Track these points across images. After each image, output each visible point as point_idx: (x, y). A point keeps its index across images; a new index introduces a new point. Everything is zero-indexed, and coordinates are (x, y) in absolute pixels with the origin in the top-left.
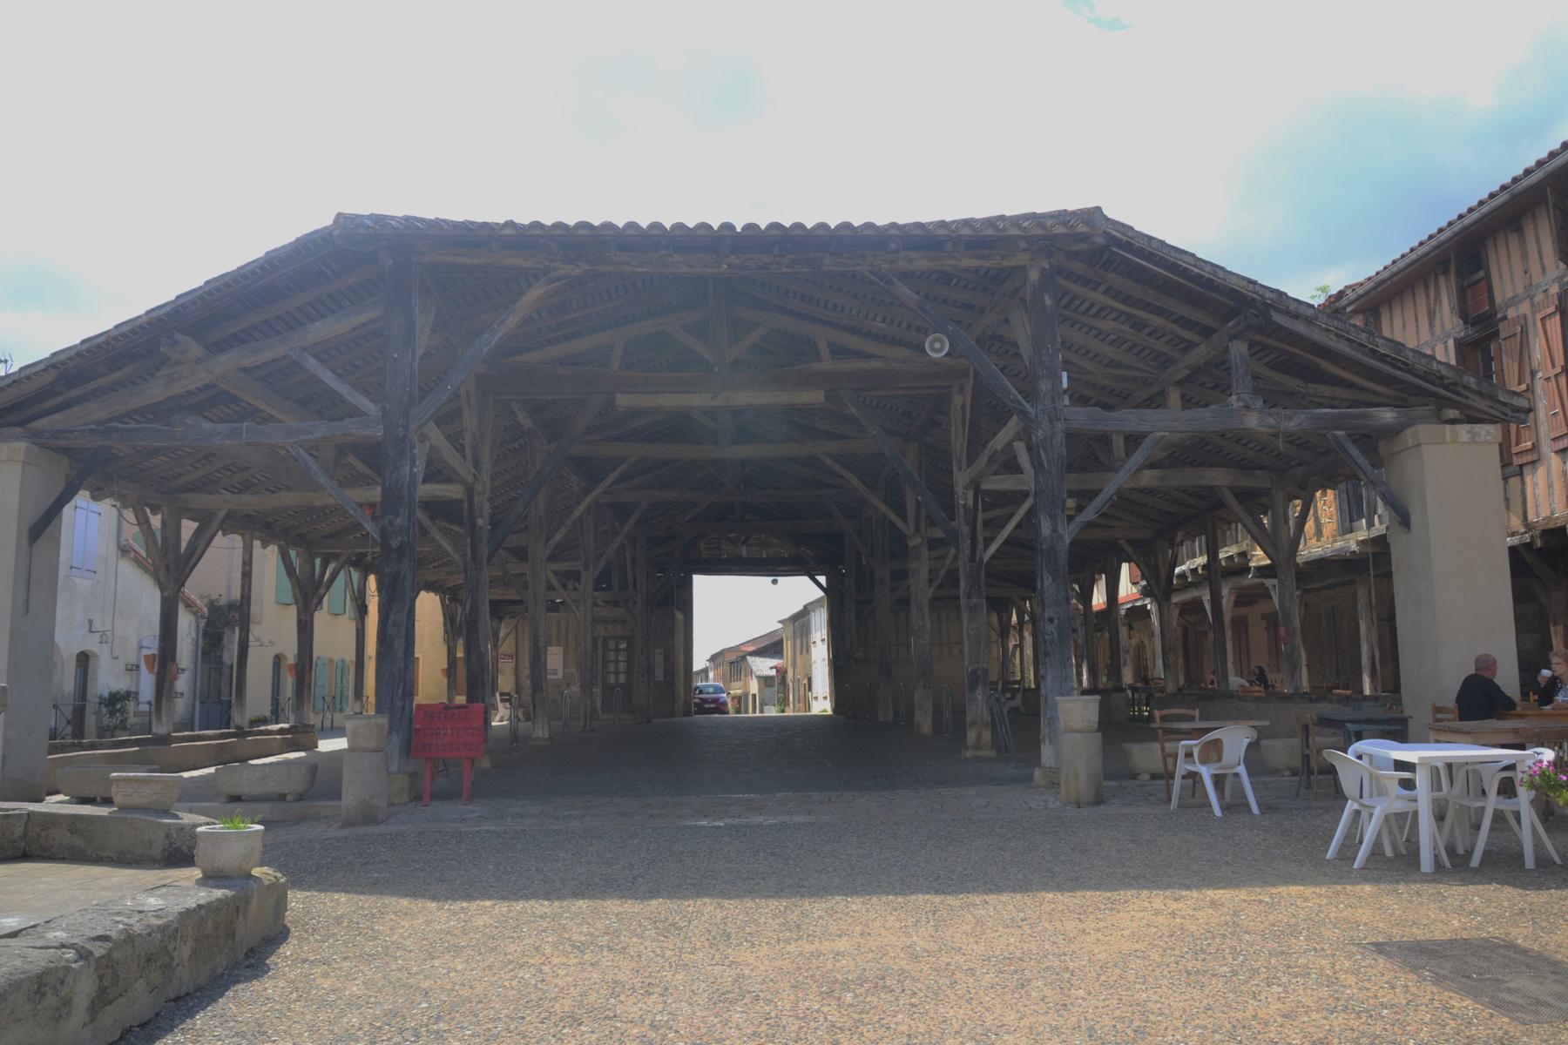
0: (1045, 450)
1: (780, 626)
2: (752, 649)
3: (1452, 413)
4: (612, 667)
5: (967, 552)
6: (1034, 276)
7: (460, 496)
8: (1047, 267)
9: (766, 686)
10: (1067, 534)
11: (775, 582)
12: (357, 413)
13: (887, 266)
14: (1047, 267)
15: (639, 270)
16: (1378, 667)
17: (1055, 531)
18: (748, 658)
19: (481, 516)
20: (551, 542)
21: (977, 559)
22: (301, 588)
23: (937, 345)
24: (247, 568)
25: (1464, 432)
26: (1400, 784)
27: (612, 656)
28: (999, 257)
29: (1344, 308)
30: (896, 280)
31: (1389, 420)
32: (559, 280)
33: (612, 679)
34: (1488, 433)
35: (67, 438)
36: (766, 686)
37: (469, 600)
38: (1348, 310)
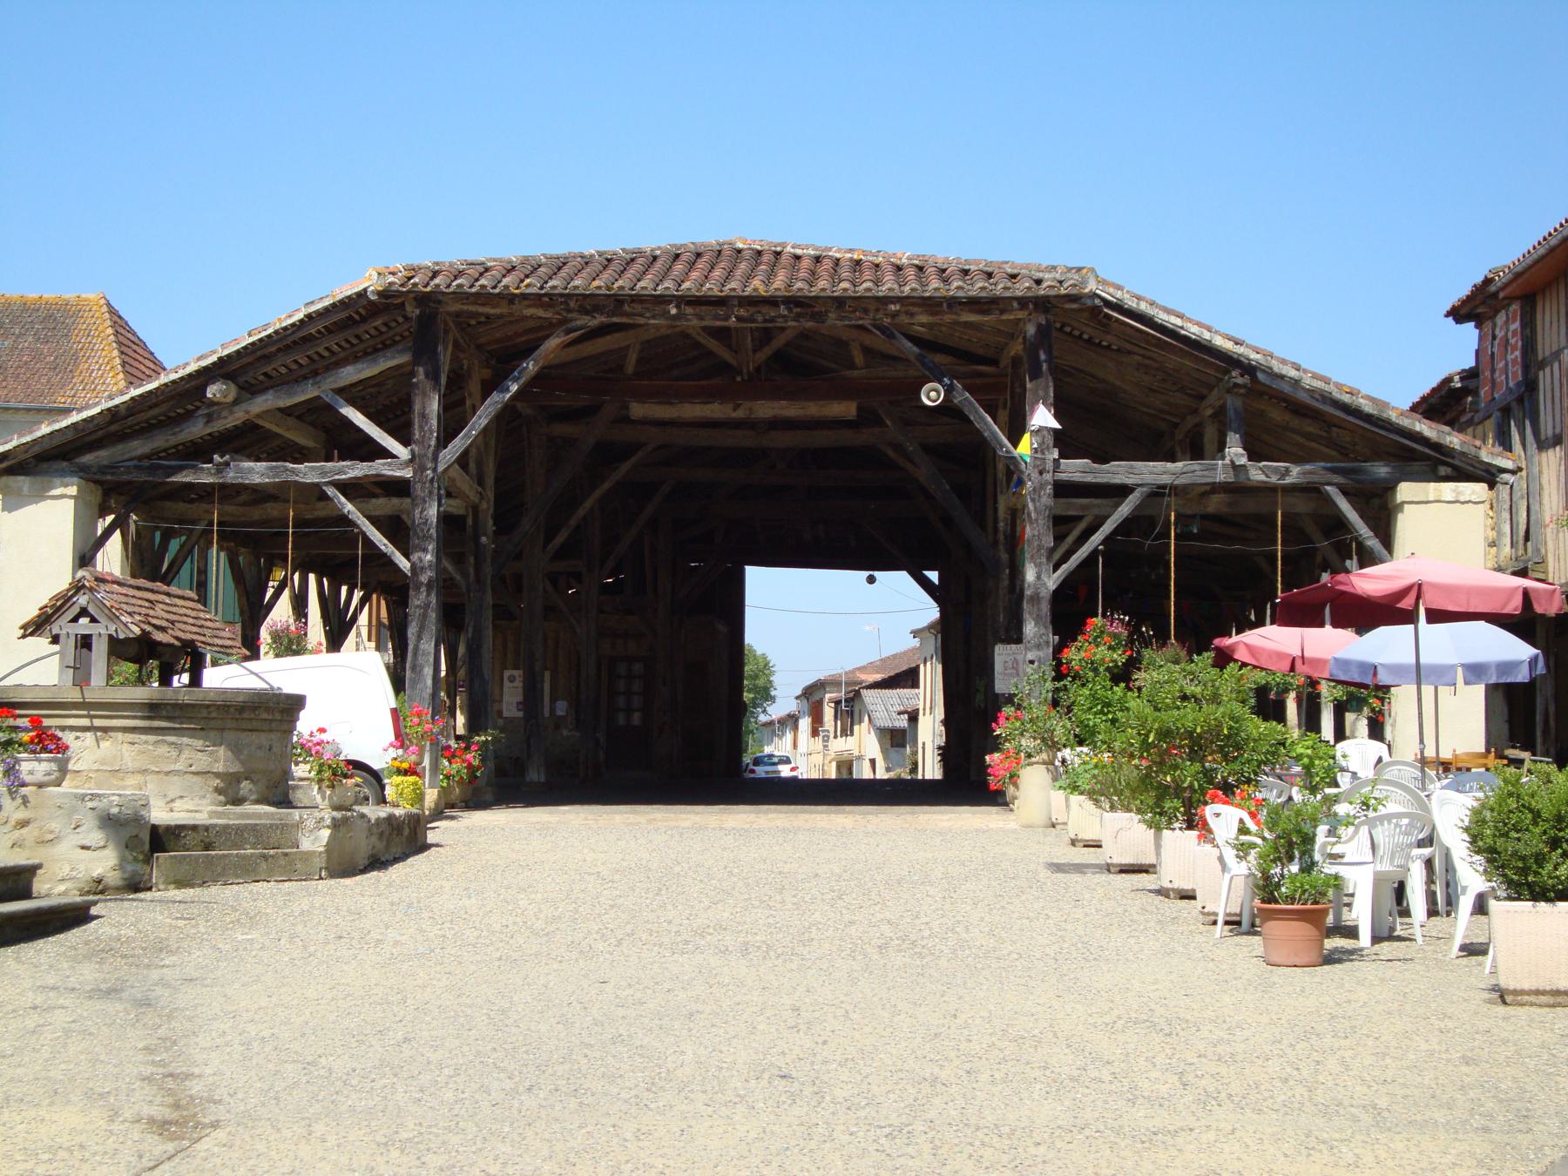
0: (1033, 500)
1: (916, 642)
2: (878, 677)
3: (1443, 470)
4: (621, 701)
5: (1006, 583)
6: (1031, 330)
7: (462, 512)
8: (1044, 322)
9: (892, 746)
10: (1052, 582)
11: (871, 580)
12: (385, 453)
13: (889, 320)
14: (1044, 322)
15: (652, 321)
16: (1552, 723)
17: (1039, 577)
18: (864, 692)
19: (485, 535)
20: (550, 546)
21: (1018, 590)
22: (247, 594)
23: (933, 394)
24: (203, 577)
25: (1448, 491)
26: (338, 650)
27: (621, 686)
28: (997, 312)
29: (1497, 293)
30: (898, 335)
31: (1383, 475)
32: (575, 331)
33: (621, 719)
34: (1473, 492)
35: (113, 474)
36: (892, 746)
37: (472, 624)
38: (1501, 295)
